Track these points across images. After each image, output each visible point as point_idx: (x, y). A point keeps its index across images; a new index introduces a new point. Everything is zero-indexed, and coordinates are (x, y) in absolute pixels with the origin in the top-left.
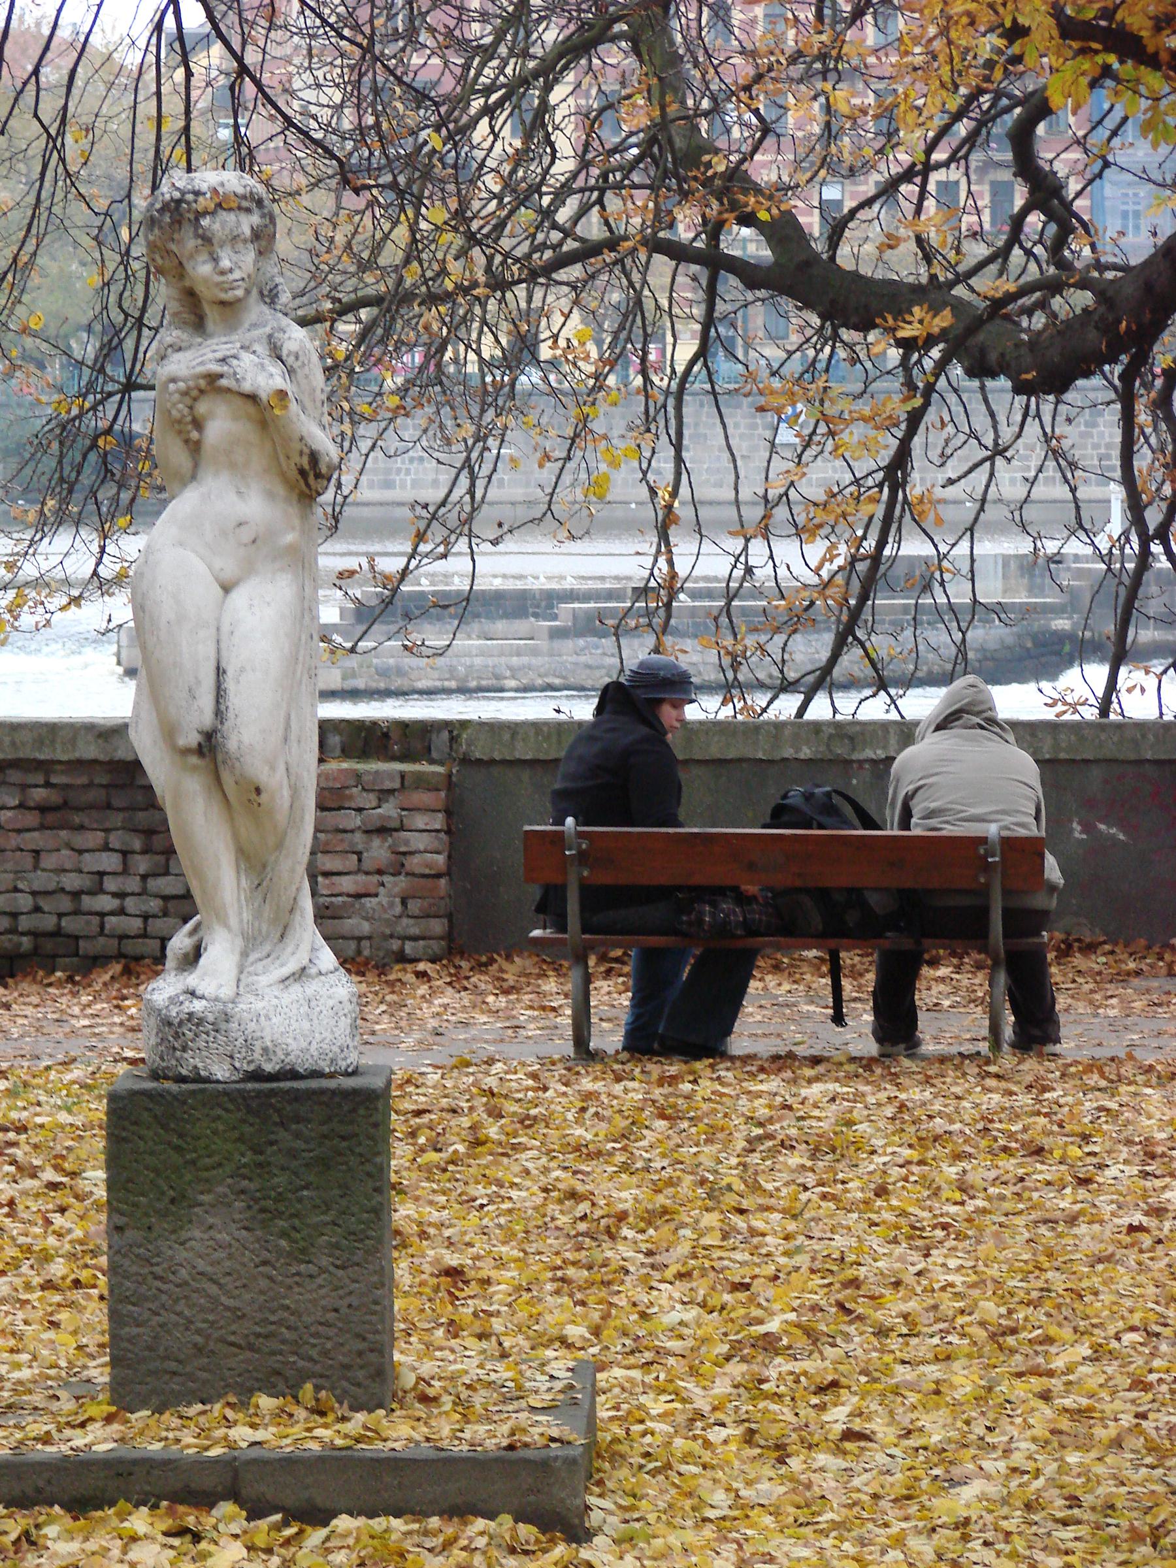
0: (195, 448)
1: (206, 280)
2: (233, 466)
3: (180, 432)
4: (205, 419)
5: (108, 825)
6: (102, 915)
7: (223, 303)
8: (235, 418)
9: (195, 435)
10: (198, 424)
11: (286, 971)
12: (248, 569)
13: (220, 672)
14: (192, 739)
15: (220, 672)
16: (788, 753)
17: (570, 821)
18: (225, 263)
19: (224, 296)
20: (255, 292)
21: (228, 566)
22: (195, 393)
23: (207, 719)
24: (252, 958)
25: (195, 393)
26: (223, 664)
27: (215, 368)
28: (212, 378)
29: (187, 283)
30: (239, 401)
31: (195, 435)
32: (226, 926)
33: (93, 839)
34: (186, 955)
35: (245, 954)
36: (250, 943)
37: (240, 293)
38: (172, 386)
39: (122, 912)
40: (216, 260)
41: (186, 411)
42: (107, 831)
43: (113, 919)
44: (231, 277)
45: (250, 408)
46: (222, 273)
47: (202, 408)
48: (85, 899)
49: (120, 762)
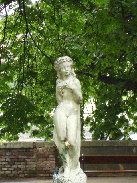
0: (62, 97)
1: (64, 72)
2: (68, 99)
3: (60, 94)
4: (64, 92)
5: (6, 157)
6: (5, 171)
7: (66, 76)
8: (68, 92)
9: (62, 95)
10: (62, 93)
11: (77, 173)
12: (70, 114)
13: (67, 129)
14: (63, 139)
15: (67, 129)
16: (104, 145)
17: (83, 155)
18: (67, 70)
19: (66, 74)
20: (71, 74)
21: (68, 114)
22: (62, 89)
23: (65, 135)
24: (72, 171)
25: (62, 89)
26: (67, 128)
27: (66, 85)
28: (65, 86)
29: (61, 73)
30: (69, 90)
31: (62, 95)
32: (68, 167)
33: (4, 160)
34: (61, 171)
35: (70, 171)
36: (71, 169)
37: (69, 74)
38: (59, 88)
39: (8, 170)
40: (65, 69)
41: (61, 91)
42: (6, 158)
43: (7, 171)
44: (67, 72)
45: (71, 91)
46: (66, 71)
47: (63, 90)
48: (3, 169)
49: (8, 148)
